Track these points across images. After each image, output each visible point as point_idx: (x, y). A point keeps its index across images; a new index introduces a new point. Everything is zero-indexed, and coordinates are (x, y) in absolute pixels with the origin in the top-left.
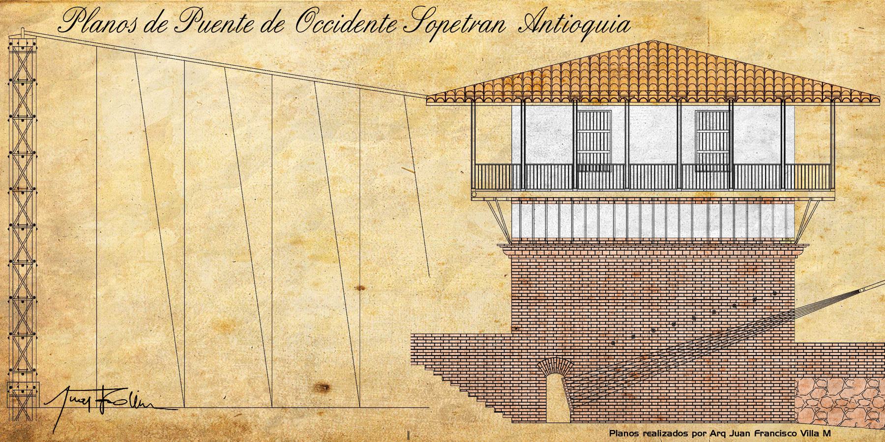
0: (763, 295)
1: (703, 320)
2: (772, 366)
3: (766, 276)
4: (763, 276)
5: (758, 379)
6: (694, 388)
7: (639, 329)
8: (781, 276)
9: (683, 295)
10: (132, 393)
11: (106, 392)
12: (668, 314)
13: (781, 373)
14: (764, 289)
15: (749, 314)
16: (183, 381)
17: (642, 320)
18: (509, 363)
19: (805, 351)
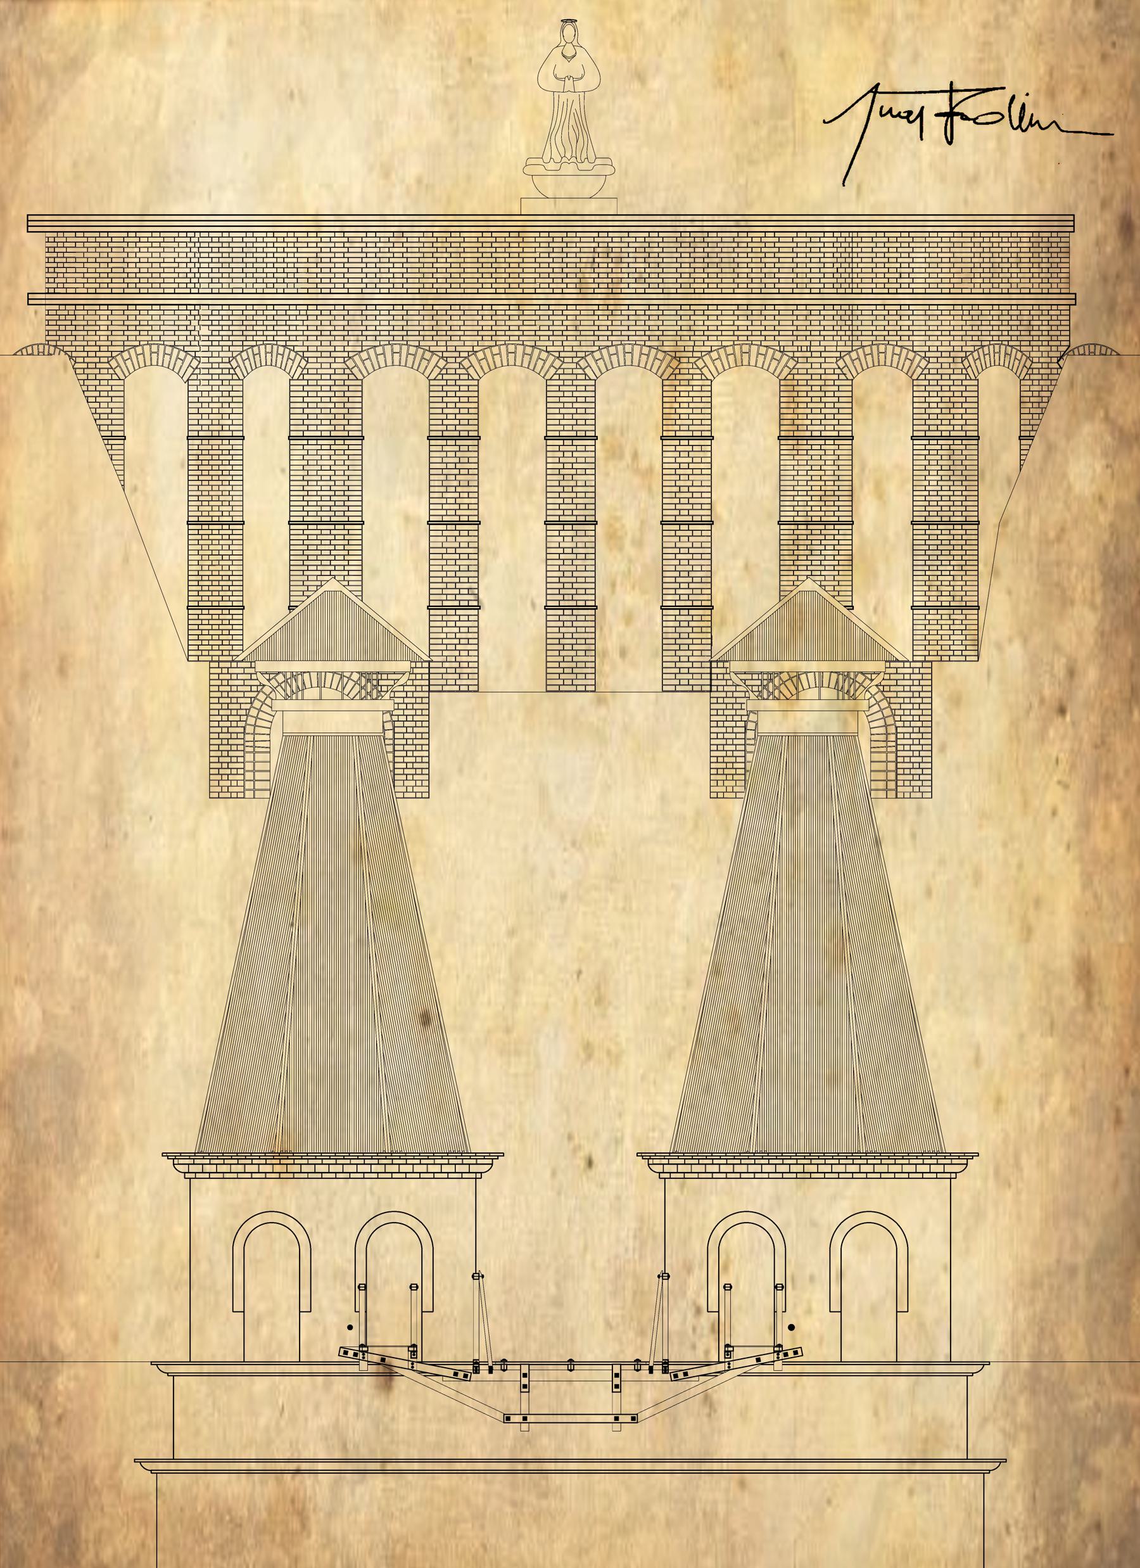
0: (808, 260)
1: (333, 553)
2: (507, 250)
3: (772, 265)
4: (405, 286)
5: (818, 260)
6: (364, 255)
7: (799, 275)
8: (521, 286)
9: (542, 275)
10: (1013, 98)
11: (957, 97)
12: (736, 270)
13: (346, 245)
14: (661, 275)
15: (328, 532)
16: (389, 1466)
17: (719, 270)
18: (517, 275)
19: (719, 255)
